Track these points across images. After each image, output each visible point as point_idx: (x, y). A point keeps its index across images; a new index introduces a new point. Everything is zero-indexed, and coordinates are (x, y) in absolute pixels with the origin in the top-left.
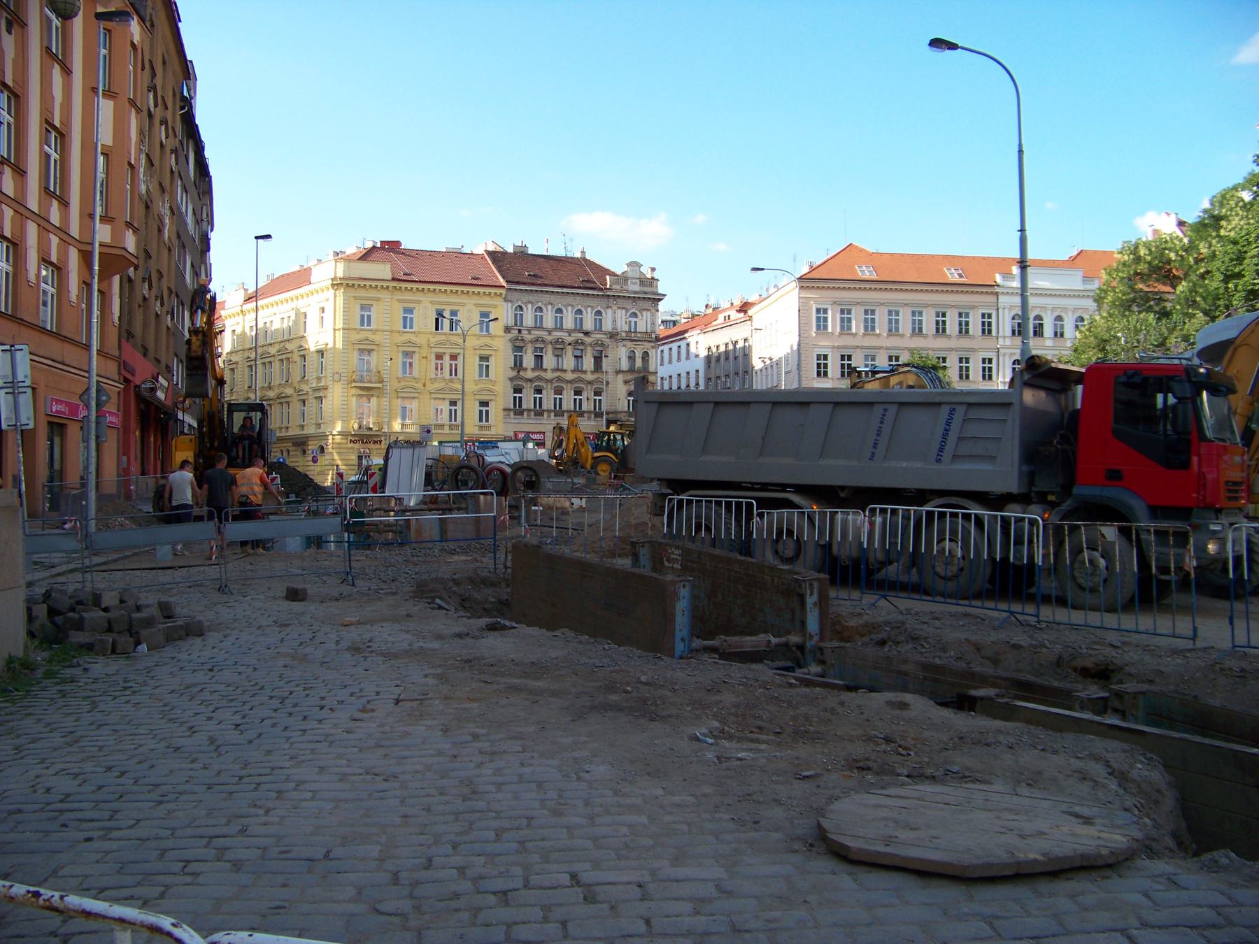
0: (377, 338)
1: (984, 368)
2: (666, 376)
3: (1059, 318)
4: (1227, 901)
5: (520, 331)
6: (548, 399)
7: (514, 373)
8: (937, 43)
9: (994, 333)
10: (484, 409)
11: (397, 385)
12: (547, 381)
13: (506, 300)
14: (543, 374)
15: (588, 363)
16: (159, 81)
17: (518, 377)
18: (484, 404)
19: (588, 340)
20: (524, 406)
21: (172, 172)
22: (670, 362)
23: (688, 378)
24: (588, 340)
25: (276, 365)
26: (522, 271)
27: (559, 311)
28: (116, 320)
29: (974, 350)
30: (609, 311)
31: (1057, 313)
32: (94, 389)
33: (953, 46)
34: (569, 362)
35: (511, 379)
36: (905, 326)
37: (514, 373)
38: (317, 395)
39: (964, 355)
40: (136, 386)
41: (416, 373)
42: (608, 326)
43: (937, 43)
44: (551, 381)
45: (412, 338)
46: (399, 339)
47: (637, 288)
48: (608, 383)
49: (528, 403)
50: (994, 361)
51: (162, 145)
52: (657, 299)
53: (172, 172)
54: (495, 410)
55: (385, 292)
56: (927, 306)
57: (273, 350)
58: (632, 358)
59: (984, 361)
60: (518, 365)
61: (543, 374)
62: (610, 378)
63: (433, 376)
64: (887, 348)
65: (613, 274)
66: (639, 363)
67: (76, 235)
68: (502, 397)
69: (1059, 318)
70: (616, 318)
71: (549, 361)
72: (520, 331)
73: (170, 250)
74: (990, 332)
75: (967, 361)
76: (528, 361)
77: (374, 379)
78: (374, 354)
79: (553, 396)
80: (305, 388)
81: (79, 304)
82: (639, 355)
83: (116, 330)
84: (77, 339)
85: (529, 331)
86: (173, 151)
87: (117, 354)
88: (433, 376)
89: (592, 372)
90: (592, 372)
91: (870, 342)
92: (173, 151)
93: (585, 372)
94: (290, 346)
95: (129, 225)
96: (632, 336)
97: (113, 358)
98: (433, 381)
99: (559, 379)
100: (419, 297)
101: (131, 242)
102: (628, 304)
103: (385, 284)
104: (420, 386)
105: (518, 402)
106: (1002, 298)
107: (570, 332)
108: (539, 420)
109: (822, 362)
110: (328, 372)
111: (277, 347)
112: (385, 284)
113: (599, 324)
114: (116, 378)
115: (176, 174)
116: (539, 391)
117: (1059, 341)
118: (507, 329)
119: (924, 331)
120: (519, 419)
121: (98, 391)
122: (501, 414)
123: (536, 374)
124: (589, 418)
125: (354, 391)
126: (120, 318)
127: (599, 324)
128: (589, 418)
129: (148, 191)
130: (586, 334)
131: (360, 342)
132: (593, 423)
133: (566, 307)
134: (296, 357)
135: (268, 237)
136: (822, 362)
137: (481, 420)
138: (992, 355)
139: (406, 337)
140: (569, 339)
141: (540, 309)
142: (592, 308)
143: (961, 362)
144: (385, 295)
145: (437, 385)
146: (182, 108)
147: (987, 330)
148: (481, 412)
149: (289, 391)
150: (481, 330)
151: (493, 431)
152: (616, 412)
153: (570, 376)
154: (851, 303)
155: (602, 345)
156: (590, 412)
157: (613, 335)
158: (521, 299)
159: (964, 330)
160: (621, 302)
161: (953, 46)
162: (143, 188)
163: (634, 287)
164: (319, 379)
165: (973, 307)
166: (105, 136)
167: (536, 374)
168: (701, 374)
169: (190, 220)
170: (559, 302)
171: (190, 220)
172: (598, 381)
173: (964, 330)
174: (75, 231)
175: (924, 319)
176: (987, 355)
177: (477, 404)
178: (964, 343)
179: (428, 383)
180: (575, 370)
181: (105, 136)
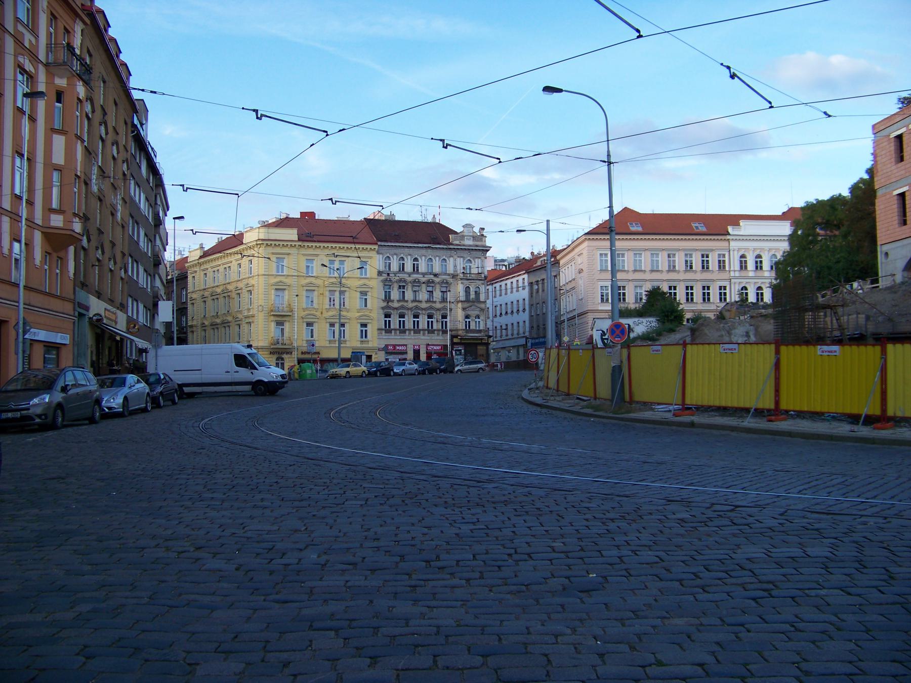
0: (287, 281)
1: (720, 293)
2: (498, 304)
3: (759, 256)
4: (857, 671)
5: (388, 274)
6: (409, 322)
7: (385, 304)
8: (548, 89)
9: (727, 268)
10: (364, 329)
11: (303, 314)
12: (408, 309)
13: (378, 253)
14: (405, 304)
15: (437, 295)
16: (108, 118)
17: (388, 307)
18: (364, 325)
19: (437, 280)
20: (392, 327)
21: (124, 174)
22: (506, 294)
23: (518, 305)
24: (437, 280)
25: (221, 300)
26: (385, 232)
27: (416, 259)
28: (72, 275)
29: (713, 281)
30: (451, 259)
31: (741, 253)
32: (21, 322)
33: (559, 91)
34: (423, 296)
35: (383, 308)
36: (680, 264)
37: (385, 304)
38: (247, 320)
39: (706, 284)
40: (90, 318)
41: (315, 306)
42: (451, 270)
43: (548, 89)
44: (411, 309)
45: (313, 280)
46: (304, 281)
47: (470, 242)
48: (451, 310)
49: (409, 325)
50: (728, 288)
51: (114, 158)
52: (486, 250)
53: (124, 174)
54: (372, 330)
55: (295, 249)
56: (679, 250)
57: (219, 290)
58: (467, 290)
59: (720, 288)
60: (387, 298)
61: (405, 304)
62: (453, 306)
63: (328, 307)
64: (684, 280)
65: (455, 233)
66: (472, 296)
67: (39, 222)
68: (376, 321)
69: (743, 256)
70: (455, 264)
71: (409, 295)
72: (388, 274)
73: (123, 227)
74: (724, 267)
75: (708, 288)
76: (395, 294)
77: (286, 309)
78: (286, 292)
79: (412, 319)
80: (240, 316)
81: (42, 266)
82: (472, 290)
83: (72, 283)
84: (41, 288)
85: (395, 274)
86: (125, 161)
87: (72, 297)
88: (328, 307)
89: (441, 302)
90: (441, 302)
91: (690, 276)
92: (125, 161)
93: (435, 302)
94: (230, 287)
95: (75, 215)
96: (466, 277)
97: (69, 300)
98: (328, 310)
99: (431, 308)
100: (317, 252)
101: (78, 227)
102: (465, 254)
103: (293, 244)
104: (318, 314)
105: (387, 324)
106: (732, 244)
107: (424, 274)
108: (403, 336)
109: (706, 291)
110: (255, 305)
111: (221, 288)
112: (293, 244)
113: (415, 269)
114: (72, 313)
115: (128, 176)
116: (416, 316)
117: (759, 273)
118: (380, 273)
119: (677, 268)
120: (387, 336)
121: (24, 324)
122: (376, 332)
123: (401, 304)
124: (438, 334)
125: (272, 318)
126: (75, 274)
127: (415, 269)
128: (438, 334)
129: (100, 190)
130: (436, 275)
131: (276, 284)
132: (441, 338)
133: (421, 257)
134: (234, 295)
135: (182, 217)
136: (690, 291)
137: (362, 337)
138: (726, 284)
139: (308, 280)
140: (423, 280)
141: (403, 259)
142: (439, 257)
143: (720, 289)
144: (294, 251)
145: (331, 313)
146: (133, 132)
147: (721, 265)
148: (362, 331)
149: (230, 318)
150: (361, 274)
151: (370, 345)
152: (457, 330)
153: (424, 305)
154: (640, 250)
155: (447, 283)
156: (438, 330)
157: (454, 276)
158: (388, 252)
159: (705, 266)
160: (460, 253)
161: (559, 91)
162: (95, 189)
163: (468, 242)
164: (249, 310)
165: (712, 250)
166: (59, 158)
167: (401, 304)
168: (527, 302)
169: (143, 205)
170: (416, 253)
171: (143, 205)
172: (445, 308)
173: (705, 266)
174: (39, 221)
175: (694, 259)
176: (723, 284)
177: (359, 325)
178: (706, 276)
179: (324, 311)
180: (415, 301)
181: (59, 158)
